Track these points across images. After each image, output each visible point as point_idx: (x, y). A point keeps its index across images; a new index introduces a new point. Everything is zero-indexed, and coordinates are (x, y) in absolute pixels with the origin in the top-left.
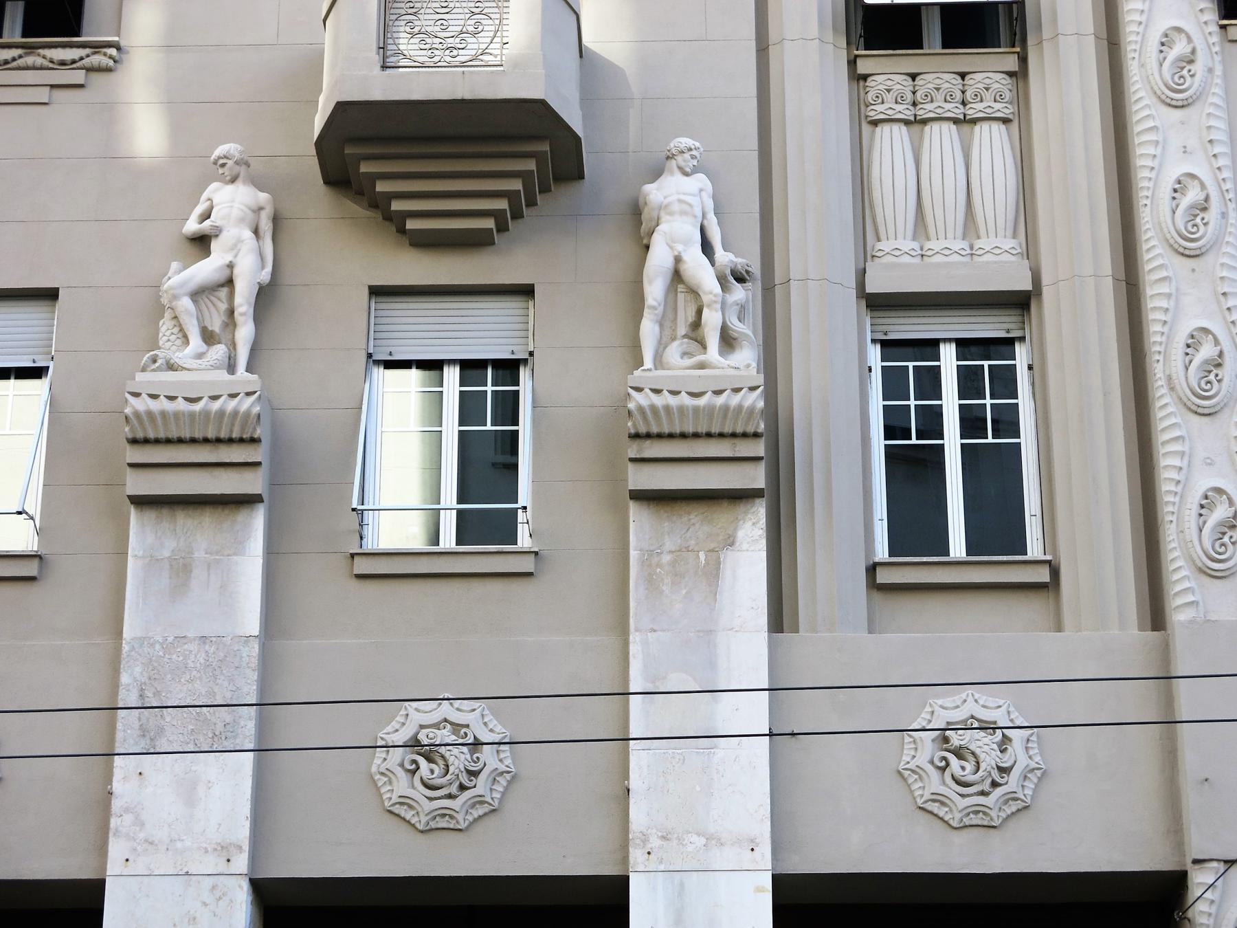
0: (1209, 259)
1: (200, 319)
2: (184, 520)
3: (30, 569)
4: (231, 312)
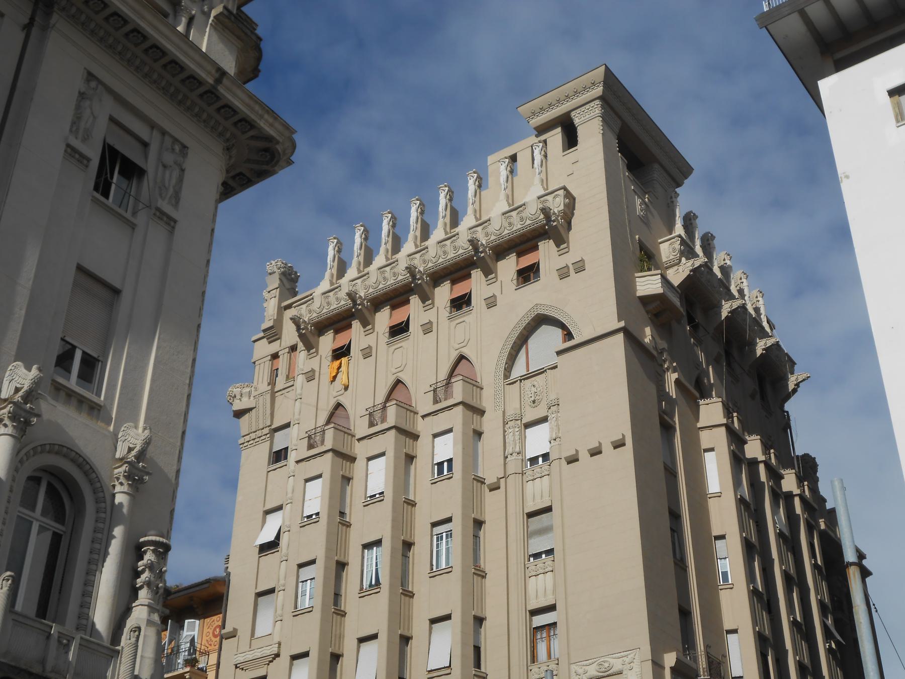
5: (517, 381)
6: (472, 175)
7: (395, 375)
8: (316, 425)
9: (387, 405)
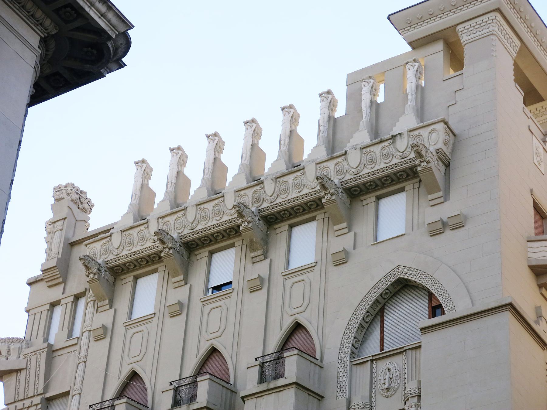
5: (368, 361)
6: (366, 80)
7: (131, 365)
8: (180, 375)
9: (198, 379)
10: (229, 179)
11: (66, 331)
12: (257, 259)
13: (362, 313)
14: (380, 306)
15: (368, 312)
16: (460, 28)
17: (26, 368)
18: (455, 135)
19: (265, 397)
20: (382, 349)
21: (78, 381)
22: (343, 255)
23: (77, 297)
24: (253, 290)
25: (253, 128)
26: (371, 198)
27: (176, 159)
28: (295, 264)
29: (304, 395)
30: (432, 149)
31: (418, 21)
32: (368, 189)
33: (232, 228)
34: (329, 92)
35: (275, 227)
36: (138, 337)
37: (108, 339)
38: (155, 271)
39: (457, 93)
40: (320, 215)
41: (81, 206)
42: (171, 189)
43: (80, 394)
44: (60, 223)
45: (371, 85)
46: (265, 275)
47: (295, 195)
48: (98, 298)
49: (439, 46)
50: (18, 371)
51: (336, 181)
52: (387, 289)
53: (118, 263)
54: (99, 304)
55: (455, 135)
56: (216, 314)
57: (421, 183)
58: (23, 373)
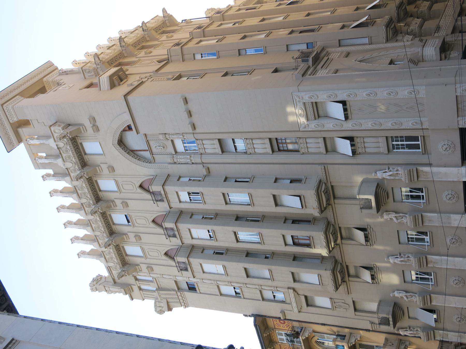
0: (382, 123)
1: (400, 219)
2: (424, 220)
3: (250, 195)
4: (399, 216)
10: (82, 218)
11: (150, 283)
12: (114, 204)
13: (133, 159)
14: (130, 152)
15: (133, 157)
16: (11, 121)
17: (166, 299)
18: (56, 122)
19: (169, 199)
20: (147, 150)
21: (170, 277)
22: (110, 168)
23: (136, 279)
24: (127, 206)
25: (60, 209)
26: (86, 157)
27: (76, 241)
28: (115, 189)
29: (167, 183)
30: (62, 132)
31: (9, 140)
32: (82, 158)
33: (102, 216)
34: (43, 177)
35: (101, 197)
36: (150, 253)
37: (152, 266)
38: (123, 247)
39: (39, 122)
40: (94, 179)
41: (99, 280)
42: (88, 242)
43: (175, 276)
44: (106, 288)
45: (38, 159)
46: (121, 201)
47: (86, 190)
48: (136, 270)
49: (20, 130)
50: (168, 302)
51: (79, 172)
52: (123, 149)
53: (120, 263)
54: (138, 270)
55: (56, 122)
56: (138, 221)
57: (78, 136)
58: (168, 300)
